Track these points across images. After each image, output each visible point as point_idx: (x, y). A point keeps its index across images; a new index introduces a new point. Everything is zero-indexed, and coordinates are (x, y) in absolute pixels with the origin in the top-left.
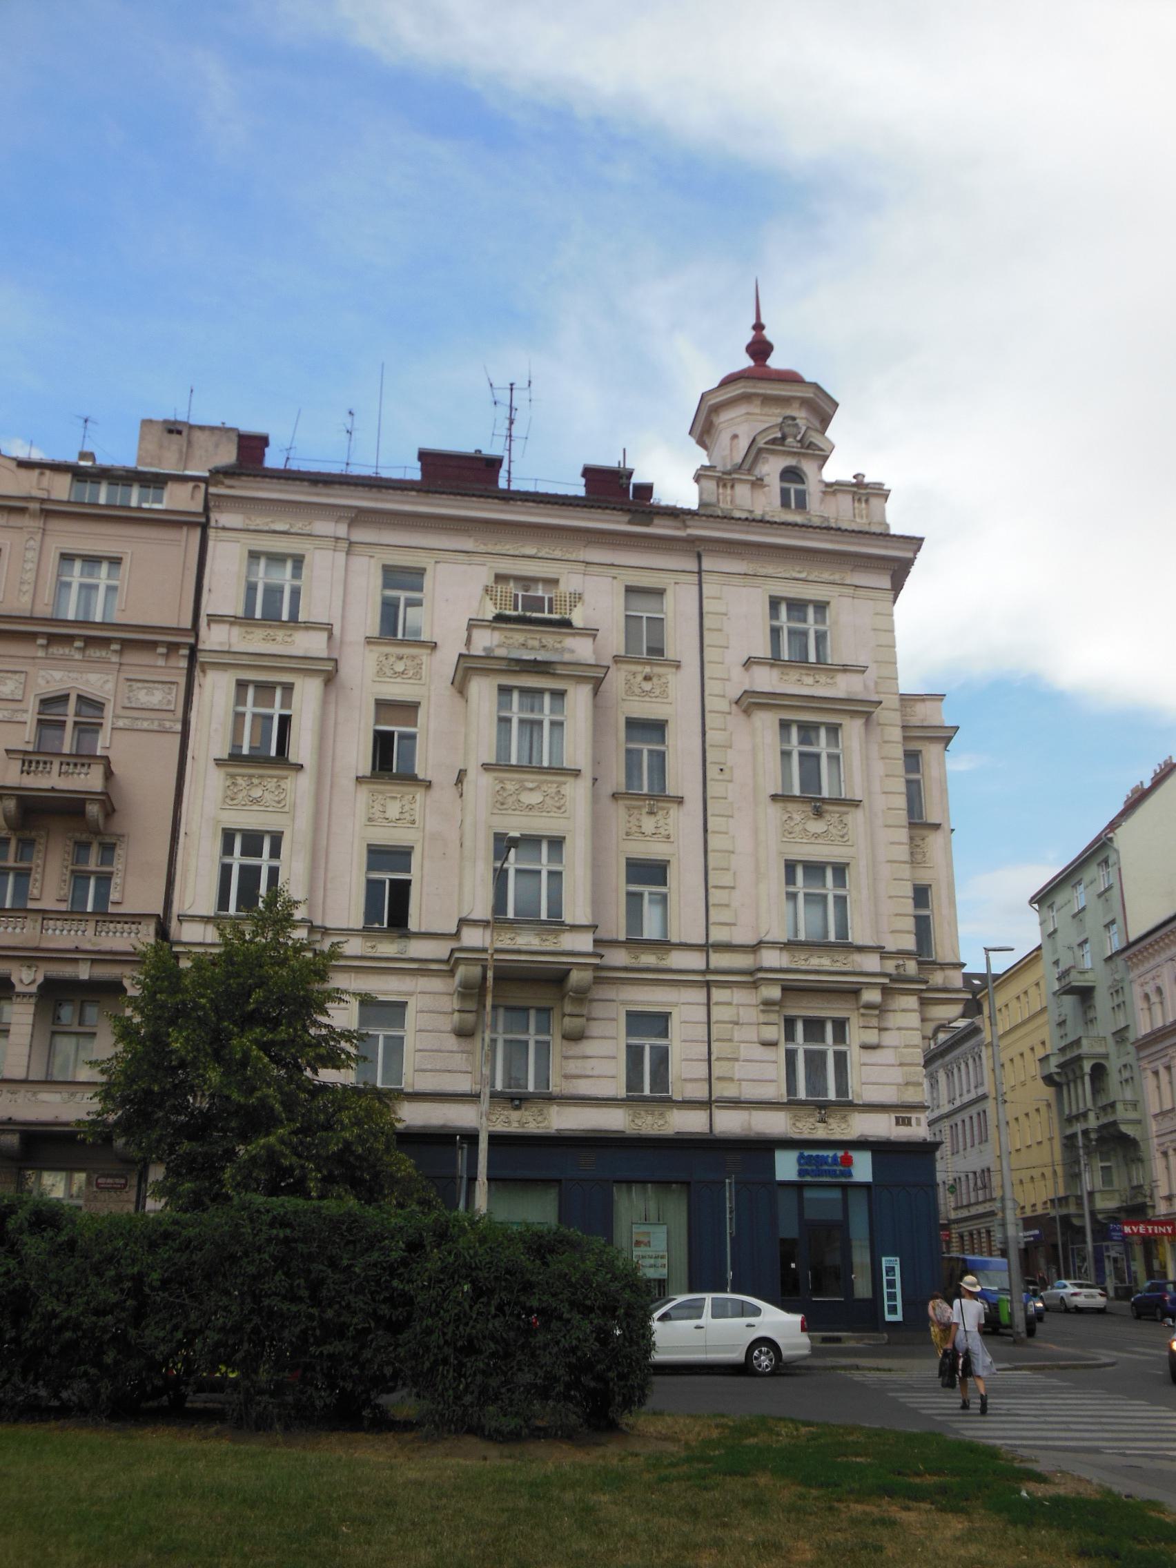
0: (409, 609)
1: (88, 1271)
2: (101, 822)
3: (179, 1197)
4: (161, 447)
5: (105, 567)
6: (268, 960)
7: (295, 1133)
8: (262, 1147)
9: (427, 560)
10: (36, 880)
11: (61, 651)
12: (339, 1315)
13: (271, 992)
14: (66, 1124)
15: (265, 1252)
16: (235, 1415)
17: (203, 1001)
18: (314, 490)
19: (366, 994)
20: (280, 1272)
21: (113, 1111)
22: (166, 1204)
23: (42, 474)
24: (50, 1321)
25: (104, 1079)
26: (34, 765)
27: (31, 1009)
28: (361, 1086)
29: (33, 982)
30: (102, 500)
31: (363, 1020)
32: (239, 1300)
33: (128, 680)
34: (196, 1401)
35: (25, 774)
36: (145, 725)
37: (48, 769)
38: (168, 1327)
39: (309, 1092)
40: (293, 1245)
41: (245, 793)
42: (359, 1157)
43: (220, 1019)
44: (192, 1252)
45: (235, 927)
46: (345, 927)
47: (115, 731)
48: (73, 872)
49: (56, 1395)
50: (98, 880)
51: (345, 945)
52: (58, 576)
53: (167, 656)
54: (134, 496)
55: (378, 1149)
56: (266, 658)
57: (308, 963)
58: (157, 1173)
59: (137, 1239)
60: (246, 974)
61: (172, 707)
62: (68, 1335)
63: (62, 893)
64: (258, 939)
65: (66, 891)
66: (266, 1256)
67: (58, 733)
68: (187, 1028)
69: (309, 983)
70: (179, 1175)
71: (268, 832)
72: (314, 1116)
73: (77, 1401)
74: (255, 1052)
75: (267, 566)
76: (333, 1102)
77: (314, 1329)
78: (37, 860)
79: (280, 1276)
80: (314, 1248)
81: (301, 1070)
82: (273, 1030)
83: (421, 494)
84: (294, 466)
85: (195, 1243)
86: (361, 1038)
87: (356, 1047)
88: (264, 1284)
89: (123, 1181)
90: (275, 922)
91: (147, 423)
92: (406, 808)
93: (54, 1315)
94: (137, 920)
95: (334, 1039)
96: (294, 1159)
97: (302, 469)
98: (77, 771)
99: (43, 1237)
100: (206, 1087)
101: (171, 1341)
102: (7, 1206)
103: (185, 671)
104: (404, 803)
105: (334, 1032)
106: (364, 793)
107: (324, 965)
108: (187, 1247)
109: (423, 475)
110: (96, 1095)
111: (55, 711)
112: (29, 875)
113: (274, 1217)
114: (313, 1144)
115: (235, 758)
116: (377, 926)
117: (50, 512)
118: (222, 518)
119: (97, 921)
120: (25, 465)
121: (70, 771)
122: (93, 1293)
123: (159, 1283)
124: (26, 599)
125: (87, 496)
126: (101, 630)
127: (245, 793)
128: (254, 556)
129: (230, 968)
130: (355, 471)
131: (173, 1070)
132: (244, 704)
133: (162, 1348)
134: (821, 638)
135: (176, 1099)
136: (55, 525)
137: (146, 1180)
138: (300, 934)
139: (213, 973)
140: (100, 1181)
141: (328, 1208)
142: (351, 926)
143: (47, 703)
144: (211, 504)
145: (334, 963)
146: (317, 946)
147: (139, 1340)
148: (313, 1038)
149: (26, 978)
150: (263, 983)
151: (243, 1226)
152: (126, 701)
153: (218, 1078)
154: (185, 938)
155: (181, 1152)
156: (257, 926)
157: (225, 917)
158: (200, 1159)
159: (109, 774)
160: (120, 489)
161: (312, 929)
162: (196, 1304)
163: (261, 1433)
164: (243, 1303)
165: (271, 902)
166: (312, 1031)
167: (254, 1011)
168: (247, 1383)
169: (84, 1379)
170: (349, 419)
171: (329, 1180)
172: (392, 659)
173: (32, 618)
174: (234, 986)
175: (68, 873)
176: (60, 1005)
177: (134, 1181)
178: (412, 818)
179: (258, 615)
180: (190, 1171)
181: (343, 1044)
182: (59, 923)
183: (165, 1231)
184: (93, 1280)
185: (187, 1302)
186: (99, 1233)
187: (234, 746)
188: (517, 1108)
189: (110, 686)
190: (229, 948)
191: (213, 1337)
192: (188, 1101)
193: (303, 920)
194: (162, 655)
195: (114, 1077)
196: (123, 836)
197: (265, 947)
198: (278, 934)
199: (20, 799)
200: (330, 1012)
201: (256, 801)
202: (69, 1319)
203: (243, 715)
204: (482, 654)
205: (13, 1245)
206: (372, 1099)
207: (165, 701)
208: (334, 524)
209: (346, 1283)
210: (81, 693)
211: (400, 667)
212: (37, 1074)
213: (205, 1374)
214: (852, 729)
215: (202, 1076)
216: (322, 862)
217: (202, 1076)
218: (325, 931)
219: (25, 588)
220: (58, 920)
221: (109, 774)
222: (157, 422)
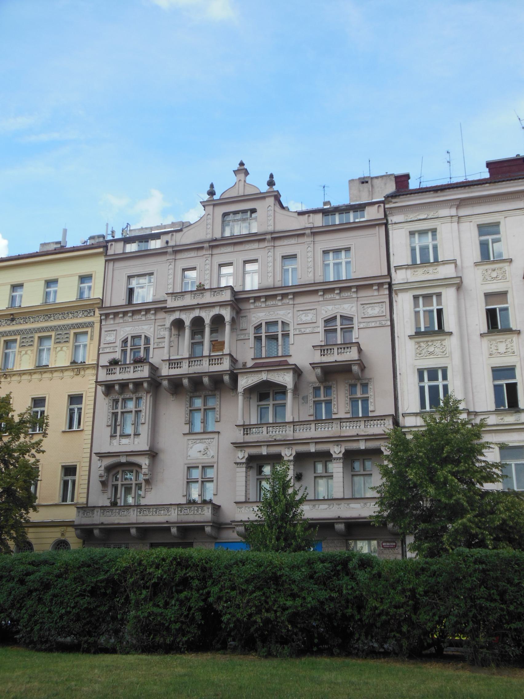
0: (494, 244)
1: (389, 587)
2: (360, 374)
3: (423, 551)
4: (360, 191)
5: (343, 253)
6: (450, 431)
7: (476, 516)
8: (460, 525)
9: (500, 217)
10: (334, 405)
11: (330, 296)
12: (517, 608)
13: (453, 446)
14: (365, 518)
15: (473, 577)
16: (470, 658)
17: (421, 454)
19: (502, 444)
20: (483, 587)
21: (385, 510)
22: (417, 554)
23: (309, 216)
24: (375, 611)
25: (378, 495)
26: (326, 351)
27: (341, 465)
28: (507, 490)
29: (291, 455)
30: (337, 222)
31: (502, 457)
32: (464, 601)
33: (362, 304)
34: (449, 651)
35: (322, 356)
36: (373, 325)
37: (332, 352)
38: (431, 614)
39: (480, 495)
40: (488, 573)
41: (425, 350)
42: (511, 527)
43: (430, 462)
44: (437, 577)
45: (431, 416)
46: (486, 410)
47: (359, 330)
48: (350, 399)
49: (382, 646)
50: (362, 401)
51: (488, 419)
52: (323, 261)
53: (378, 290)
54: (351, 217)
55: (521, 523)
56: (426, 283)
57: (469, 431)
58: (410, 540)
59: (409, 571)
60: (440, 439)
61: (384, 314)
62: (384, 617)
63: (347, 409)
64: (443, 421)
65: (349, 408)
66: (474, 579)
67: (334, 334)
68: (415, 468)
69: (472, 440)
70: (421, 540)
71: (440, 368)
72: (485, 507)
73: (392, 649)
74: (450, 477)
75: (419, 237)
76: (493, 499)
77: (505, 615)
78: (334, 396)
79: (483, 589)
80: (499, 573)
81: (474, 484)
82: (457, 466)
83: (492, 184)
84: (424, 185)
85: (437, 573)
86: (503, 466)
87: (501, 471)
88: (475, 592)
89: (394, 544)
90: (450, 412)
91: (351, 181)
92: (509, 346)
93: (376, 608)
94: (383, 418)
95: (489, 468)
96: (478, 530)
97: (428, 186)
98: (345, 351)
99: (366, 572)
100: (428, 496)
101: (432, 621)
102: (348, 557)
104: (507, 343)
105: (489, 464)
106: (485, 340)
107: (479, 431)
108: (434, 575)
109: (490, 175)
110: (376, 503)
111: (330, 325)
112: (331, 403)
113: (476, 559)
114: (486, 522)
115: (418, 334)
116: (502, 408)
117: (315, 233)
118: (393, 219)
119: (365, 421)
120: (301, 214)
121: (342, 352)
122: (393, 598)
123: (423, 592)
124: (311, 275)
126: (346, 283)
127: (425, 350)
128: (412, 233)
129: (432, 437)
130: (454, 181)
131: (410, 489)
132: (419, 307)
133: (429, 624)
135: (414, 503)
136: (318, 238)
137: (405, 544)
138: (464, 416)
139: (424, 440)
140: (384, 544)
141: (503, 553)
142: (489, 410)
143: (327, 321)
144: (388, 213)
145: (483, 429)
146: (473, 422)
147: (417, 621)
148: (478, 468)
149: (337, 451)
150: (449, 443)
151: (461, 564)
152: (363, 314)
153: (433, 491)
154: (407, 425)
155: (421, 528)
156: (442, 415)
157: (425, 412)
158: (430, 532)
159: (360, 350)
160: (344, 215)
161: (469, 413)
162: (442, 603)
163: (484, 668)
164: (466, 602)
165: (446, 403)
166: (477, 464)
167: (446, 457)
168: (474, 643)
169: (394, 639)
170: (448, 155)
171: (497, 539)
172: (489, 272)
173: (274, 288)
174: (435, 445)
175: (348, 400)
176: (354, 462)
177: (399, 544)
178: (513, 351)
179: (418, 262)
180: (426, 538)
181: (494, 470)
182: (348, 424)
183: (422, 567)
184: (392, 591)
185: (438, 601)
186: (391, 569)
187: (416, 328)
189: (354, 309)
190: (429, 427)
191: (453, 619)
192: (420, 503)
193: (464, 410)
194: (112, 318)
195: (383, 494)
196: (371, 379)
197: (447, 425)
198: (453, 417)
199: (322, 368)
200: (485, 454)
201: (431, 353)
202: (383, 610)
203: (419, 312)
205: (353, 576)
206: (513, 497)
207: (380, 312)
208: (449, 209)
209: (518, 592)
211: (494, 275)
212: (348, 495)
213: (451, 638)
215: (426, 491)
216: (469, 380)
217: (426, 491)
218: (476, 414)
220: (347, 422)
221: (360, 350)
222: (356, 180)
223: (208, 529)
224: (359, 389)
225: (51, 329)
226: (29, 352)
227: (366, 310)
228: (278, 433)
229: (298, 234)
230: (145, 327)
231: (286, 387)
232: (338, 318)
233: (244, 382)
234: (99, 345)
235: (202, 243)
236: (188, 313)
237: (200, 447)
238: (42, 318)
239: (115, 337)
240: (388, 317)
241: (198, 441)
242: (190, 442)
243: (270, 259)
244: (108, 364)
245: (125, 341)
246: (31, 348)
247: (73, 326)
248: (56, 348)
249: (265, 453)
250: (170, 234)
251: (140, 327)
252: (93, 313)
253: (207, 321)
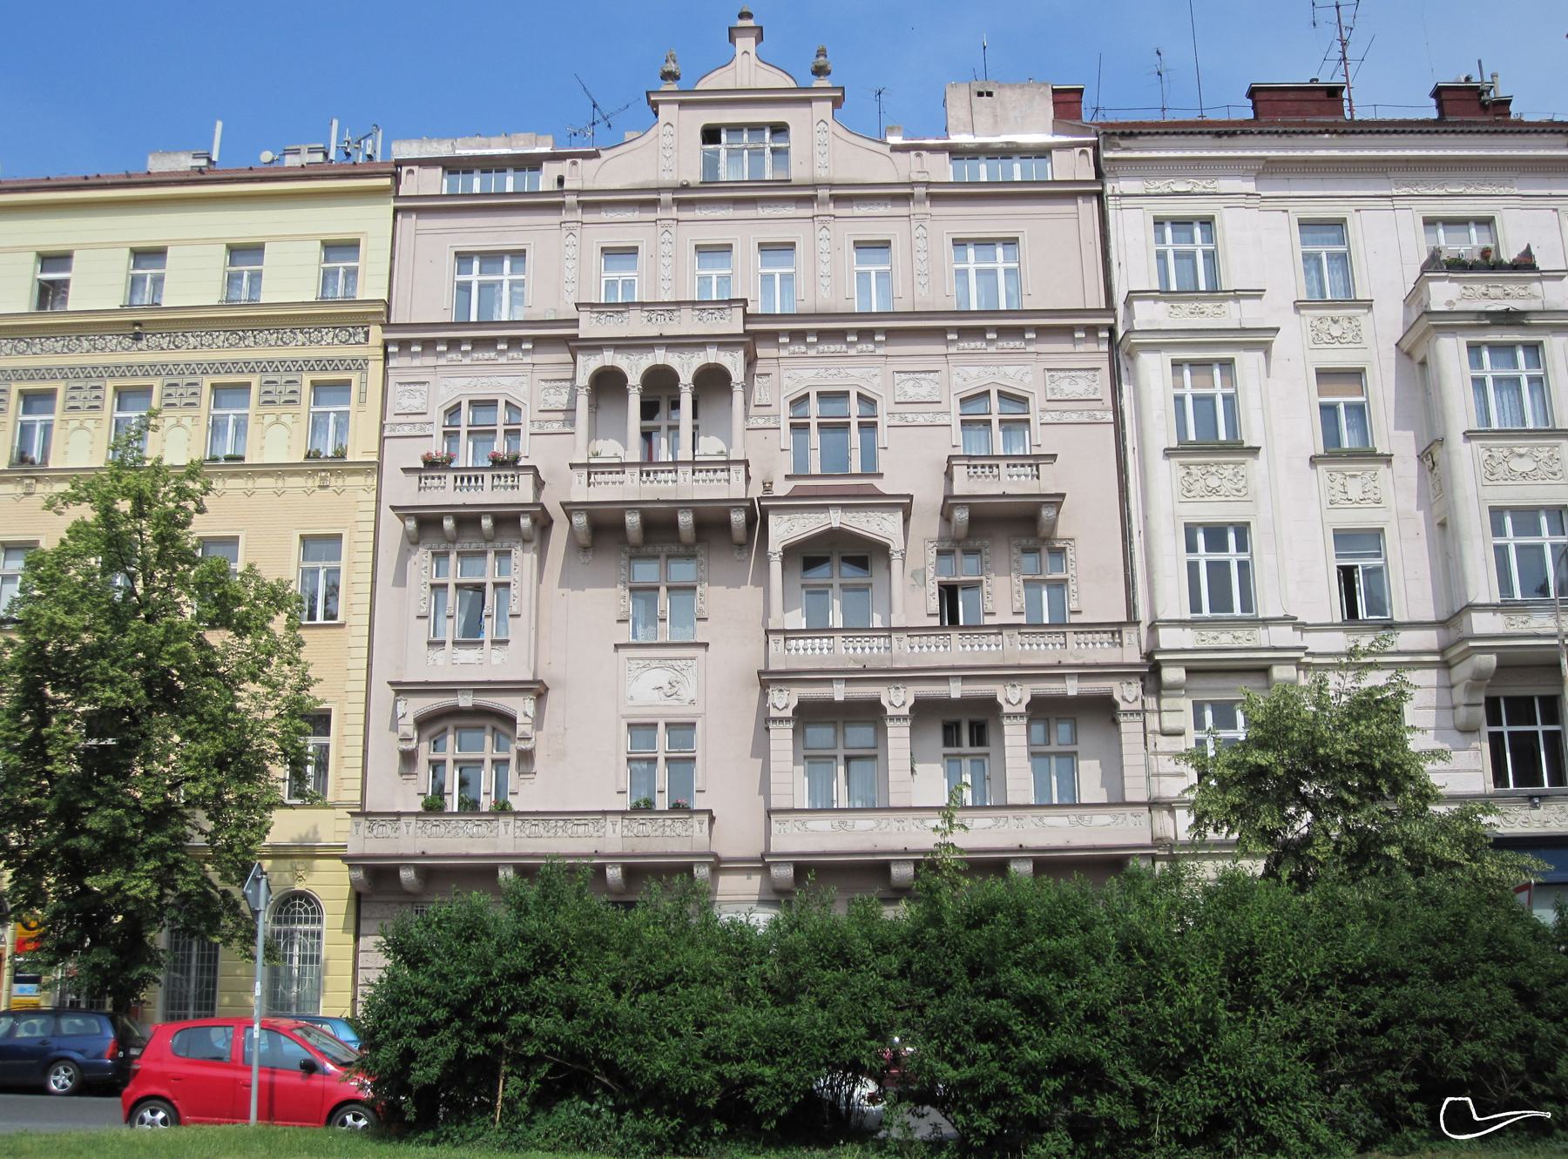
9: (1346, 208)
18: (1218, 142)
36: (1074, 417)
115: (1181, 450)
125: (746, 173)
134: (1211, 257)
144: (1105, 169)
170: (1157, 57)
188: (1535, 806)
189: (525, 388)
201: (1215, 491)
204: (1445, 308)
210: (1002, 389)
214: (1247, 363)
225: (63, 373)
226: (187, 421)
228: (870, 651)
229: (899, 195)
233: (784, 530)
234: (383, 416)
235: (658, 190)
236: (687, 356)
237: (661, 677)
238: (222, 338)
240: (1108, 402)
241: (655, 664)
244: (422, 466)
245: (454, 411)
246: (192, 412)
247: (308, 365)
248: (263, 416)
249: (839, 697)
250: (569, 161)
251: (492, 379)
253: (686, 379)
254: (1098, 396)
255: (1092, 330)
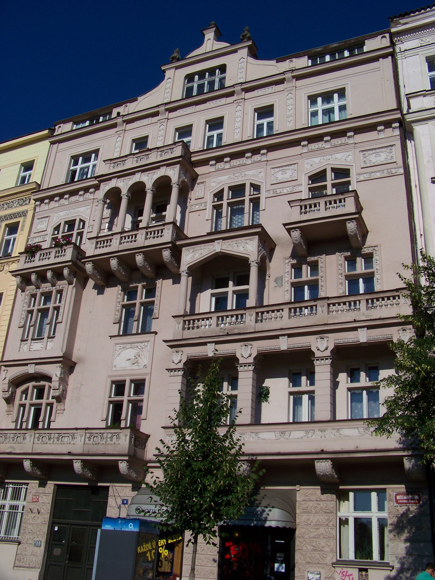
36: (378, 175)
103: (399, 137)
219: (237, 131)
223: (123, 467)
224: (360, 262)
227: (368, 157)
230: (81, 209)
231: (248, 259)
232: (330, 175)
237: (130, 353)
239: (46, 225)
241: (128, 346)
242: (118, 347)
243: (239, 114)
251: (76, 210)
252: (28, 200)
254: (394, 160)
255: (388, 124)
